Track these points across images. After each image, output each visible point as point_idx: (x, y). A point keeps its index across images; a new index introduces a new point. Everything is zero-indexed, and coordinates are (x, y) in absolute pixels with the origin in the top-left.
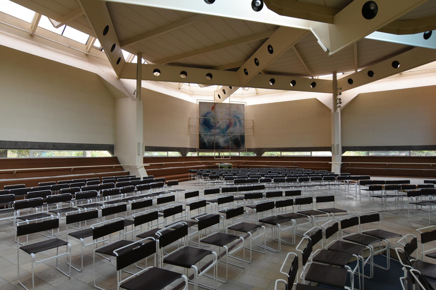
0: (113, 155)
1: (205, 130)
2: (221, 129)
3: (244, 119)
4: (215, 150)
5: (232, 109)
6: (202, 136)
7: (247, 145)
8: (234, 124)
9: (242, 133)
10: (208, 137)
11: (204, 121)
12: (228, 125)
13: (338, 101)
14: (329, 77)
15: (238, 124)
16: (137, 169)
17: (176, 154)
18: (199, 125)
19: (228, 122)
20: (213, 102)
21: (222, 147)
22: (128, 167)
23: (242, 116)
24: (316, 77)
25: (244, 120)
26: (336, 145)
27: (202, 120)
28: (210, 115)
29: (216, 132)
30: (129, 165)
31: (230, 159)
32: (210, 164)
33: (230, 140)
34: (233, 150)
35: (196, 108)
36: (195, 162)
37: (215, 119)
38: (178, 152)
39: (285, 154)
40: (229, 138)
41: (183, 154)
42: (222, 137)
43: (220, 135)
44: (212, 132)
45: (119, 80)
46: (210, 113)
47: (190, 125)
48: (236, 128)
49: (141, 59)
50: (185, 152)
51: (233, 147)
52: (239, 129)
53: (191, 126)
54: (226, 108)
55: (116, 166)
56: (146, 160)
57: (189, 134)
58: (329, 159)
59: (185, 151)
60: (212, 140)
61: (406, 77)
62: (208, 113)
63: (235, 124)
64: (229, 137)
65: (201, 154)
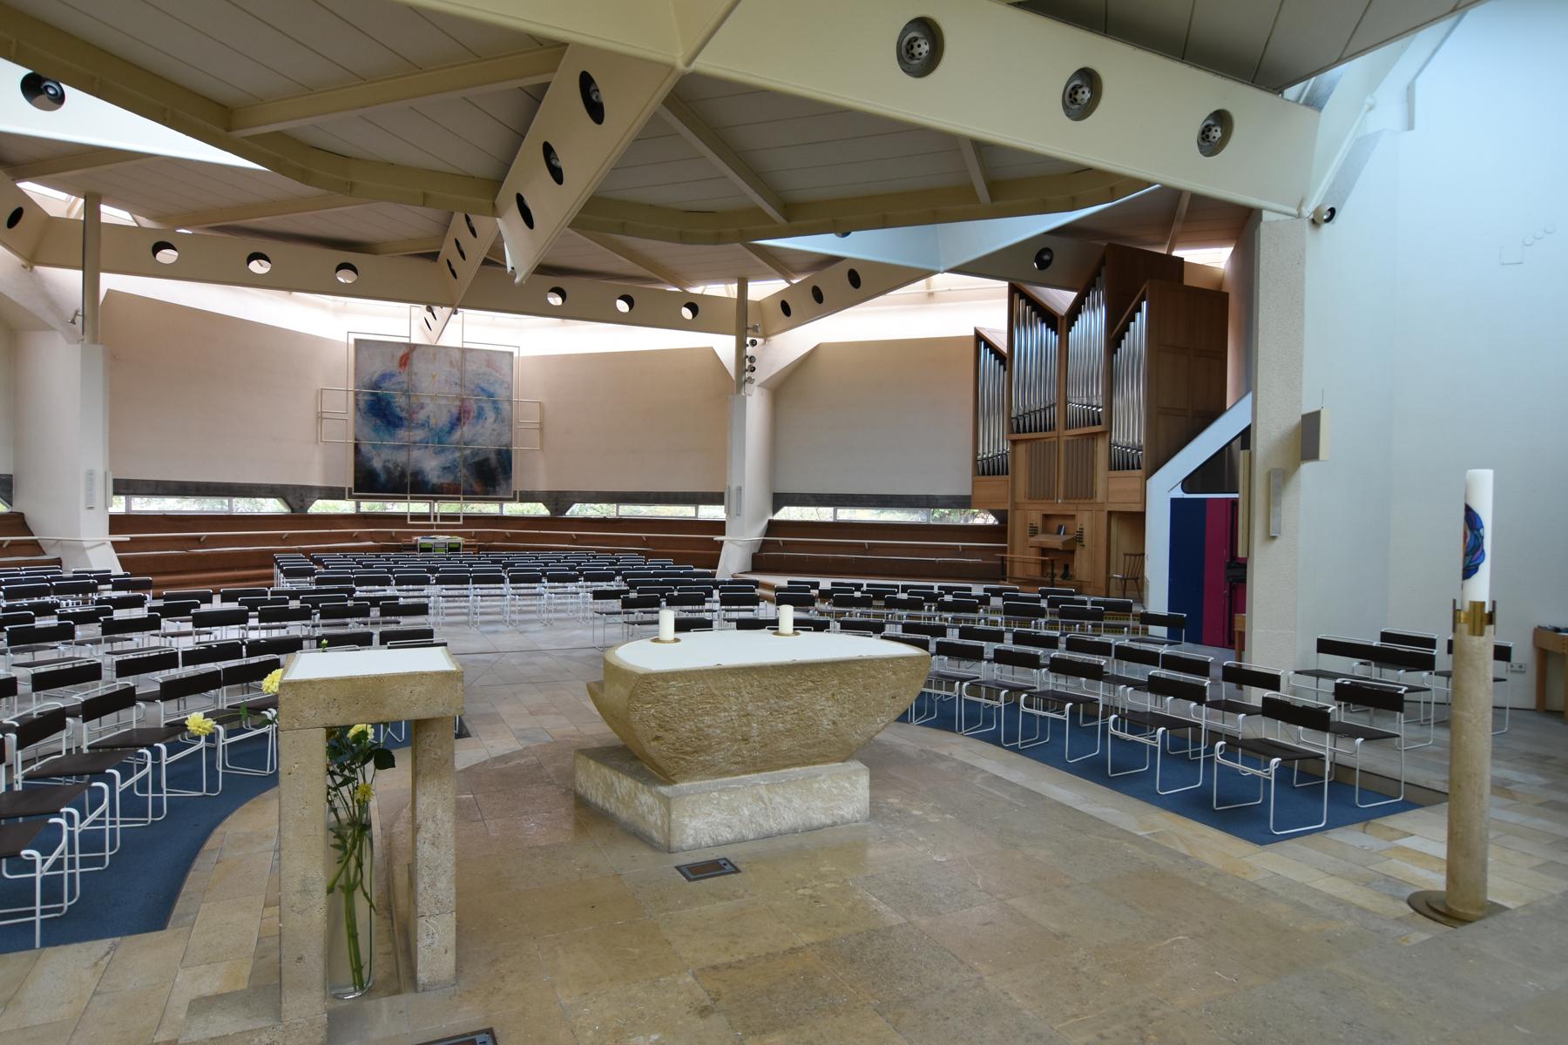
0: (11, 505)
1: (376, 429)
2: (431, 430)
3: (510, 401)
4: (409, 496)
5: (471, 367)
6: (363, 449)
7: (519, 481)
8: (475, 414)
9: (504, 444)
10: (386, 454)
11: (373, 401)
12: (456, 416)
13: (748, 363)
14: (725, 290)
15: (490, 415)
16: (84, 549)
17: (273, 506)
18: (356, 414)
19: (456, 406)
20: (407, 341)
21: (434, 485)
22: (55, 544)
23: (506, 388)
24: (697, 290)
25: (511, 401)
26: (734, 487)
27: (366, 398)
28: (393, 384)
29: (412, 440)
30: (59, 538)
31: (461, 522)
32: (393, 539)
33: (461, 464)
34: (471, 496)
35: (345, 358)
36: (333, 531)
37: (409, 396)
38: (276, 500)
39: (846, 514)
40: (460, 457)
41: (294, 506)
42: (436, 453)
43: (427, 447)
44: (400, 436)
45: (29, 269)
46: (394, 375)
47: (322, 412)
48: (483, 427)
49: (99, 207)
50: (303, 501)
51: (471, 486)
52: (494, 430)
53: (324, 415)
54: (451, 362)
55: (12, 541)
56: (118, 523)
57: (320, 443)
58: (719, 527)
59: (301, 495)
60: (401, 464)
61: (941, 305)
62: (384, 377)
63: (480, 414)
64: (457, 454)
65: (367, 507)
